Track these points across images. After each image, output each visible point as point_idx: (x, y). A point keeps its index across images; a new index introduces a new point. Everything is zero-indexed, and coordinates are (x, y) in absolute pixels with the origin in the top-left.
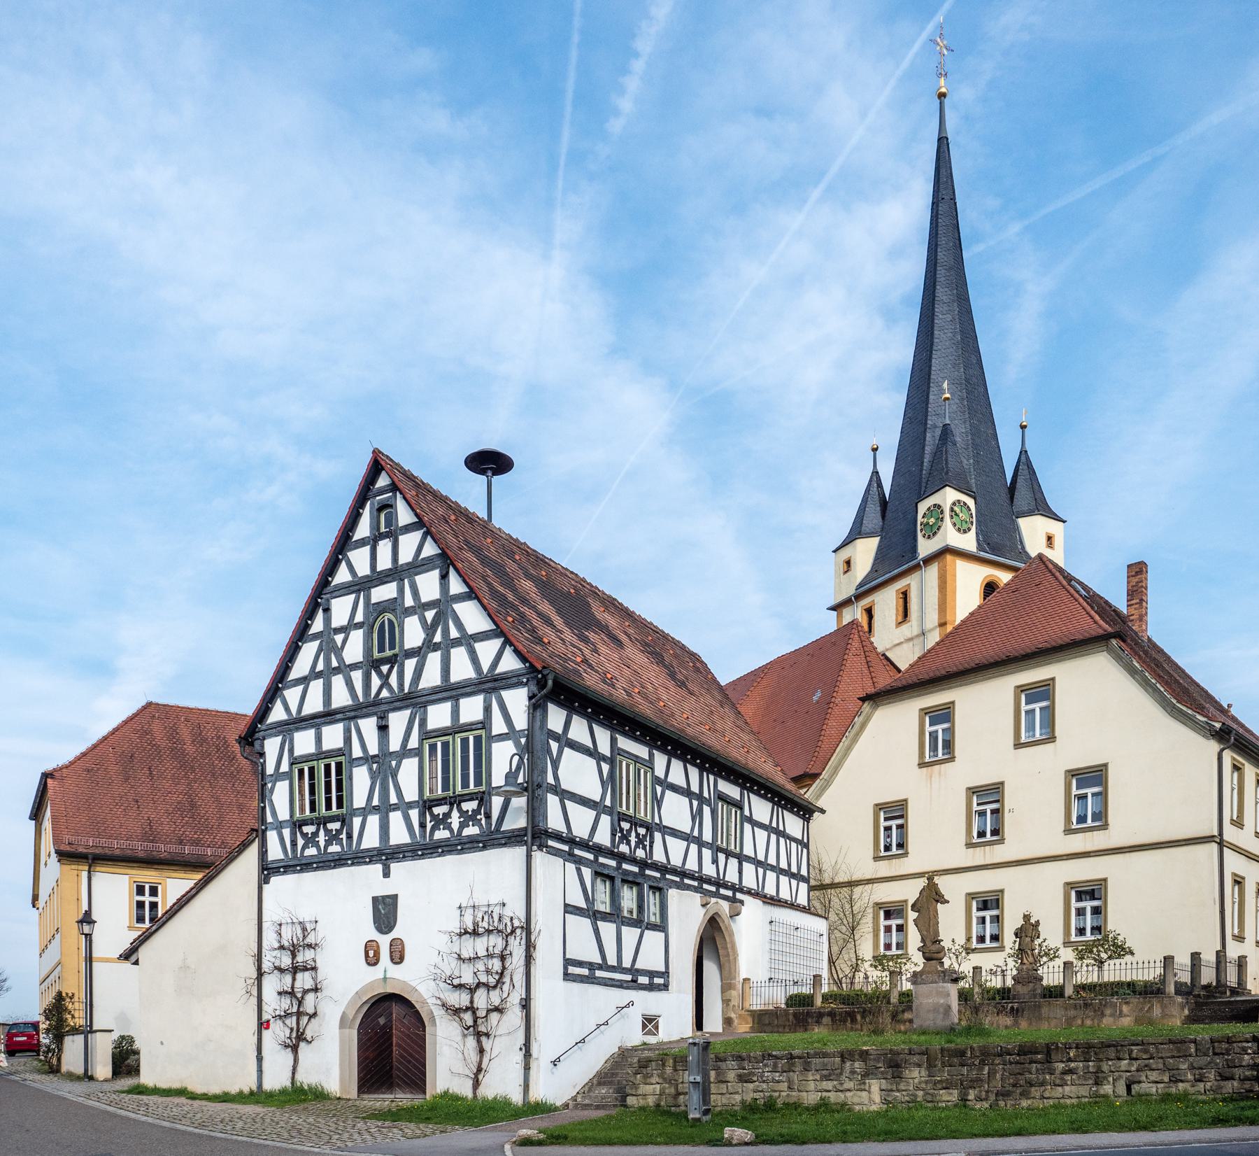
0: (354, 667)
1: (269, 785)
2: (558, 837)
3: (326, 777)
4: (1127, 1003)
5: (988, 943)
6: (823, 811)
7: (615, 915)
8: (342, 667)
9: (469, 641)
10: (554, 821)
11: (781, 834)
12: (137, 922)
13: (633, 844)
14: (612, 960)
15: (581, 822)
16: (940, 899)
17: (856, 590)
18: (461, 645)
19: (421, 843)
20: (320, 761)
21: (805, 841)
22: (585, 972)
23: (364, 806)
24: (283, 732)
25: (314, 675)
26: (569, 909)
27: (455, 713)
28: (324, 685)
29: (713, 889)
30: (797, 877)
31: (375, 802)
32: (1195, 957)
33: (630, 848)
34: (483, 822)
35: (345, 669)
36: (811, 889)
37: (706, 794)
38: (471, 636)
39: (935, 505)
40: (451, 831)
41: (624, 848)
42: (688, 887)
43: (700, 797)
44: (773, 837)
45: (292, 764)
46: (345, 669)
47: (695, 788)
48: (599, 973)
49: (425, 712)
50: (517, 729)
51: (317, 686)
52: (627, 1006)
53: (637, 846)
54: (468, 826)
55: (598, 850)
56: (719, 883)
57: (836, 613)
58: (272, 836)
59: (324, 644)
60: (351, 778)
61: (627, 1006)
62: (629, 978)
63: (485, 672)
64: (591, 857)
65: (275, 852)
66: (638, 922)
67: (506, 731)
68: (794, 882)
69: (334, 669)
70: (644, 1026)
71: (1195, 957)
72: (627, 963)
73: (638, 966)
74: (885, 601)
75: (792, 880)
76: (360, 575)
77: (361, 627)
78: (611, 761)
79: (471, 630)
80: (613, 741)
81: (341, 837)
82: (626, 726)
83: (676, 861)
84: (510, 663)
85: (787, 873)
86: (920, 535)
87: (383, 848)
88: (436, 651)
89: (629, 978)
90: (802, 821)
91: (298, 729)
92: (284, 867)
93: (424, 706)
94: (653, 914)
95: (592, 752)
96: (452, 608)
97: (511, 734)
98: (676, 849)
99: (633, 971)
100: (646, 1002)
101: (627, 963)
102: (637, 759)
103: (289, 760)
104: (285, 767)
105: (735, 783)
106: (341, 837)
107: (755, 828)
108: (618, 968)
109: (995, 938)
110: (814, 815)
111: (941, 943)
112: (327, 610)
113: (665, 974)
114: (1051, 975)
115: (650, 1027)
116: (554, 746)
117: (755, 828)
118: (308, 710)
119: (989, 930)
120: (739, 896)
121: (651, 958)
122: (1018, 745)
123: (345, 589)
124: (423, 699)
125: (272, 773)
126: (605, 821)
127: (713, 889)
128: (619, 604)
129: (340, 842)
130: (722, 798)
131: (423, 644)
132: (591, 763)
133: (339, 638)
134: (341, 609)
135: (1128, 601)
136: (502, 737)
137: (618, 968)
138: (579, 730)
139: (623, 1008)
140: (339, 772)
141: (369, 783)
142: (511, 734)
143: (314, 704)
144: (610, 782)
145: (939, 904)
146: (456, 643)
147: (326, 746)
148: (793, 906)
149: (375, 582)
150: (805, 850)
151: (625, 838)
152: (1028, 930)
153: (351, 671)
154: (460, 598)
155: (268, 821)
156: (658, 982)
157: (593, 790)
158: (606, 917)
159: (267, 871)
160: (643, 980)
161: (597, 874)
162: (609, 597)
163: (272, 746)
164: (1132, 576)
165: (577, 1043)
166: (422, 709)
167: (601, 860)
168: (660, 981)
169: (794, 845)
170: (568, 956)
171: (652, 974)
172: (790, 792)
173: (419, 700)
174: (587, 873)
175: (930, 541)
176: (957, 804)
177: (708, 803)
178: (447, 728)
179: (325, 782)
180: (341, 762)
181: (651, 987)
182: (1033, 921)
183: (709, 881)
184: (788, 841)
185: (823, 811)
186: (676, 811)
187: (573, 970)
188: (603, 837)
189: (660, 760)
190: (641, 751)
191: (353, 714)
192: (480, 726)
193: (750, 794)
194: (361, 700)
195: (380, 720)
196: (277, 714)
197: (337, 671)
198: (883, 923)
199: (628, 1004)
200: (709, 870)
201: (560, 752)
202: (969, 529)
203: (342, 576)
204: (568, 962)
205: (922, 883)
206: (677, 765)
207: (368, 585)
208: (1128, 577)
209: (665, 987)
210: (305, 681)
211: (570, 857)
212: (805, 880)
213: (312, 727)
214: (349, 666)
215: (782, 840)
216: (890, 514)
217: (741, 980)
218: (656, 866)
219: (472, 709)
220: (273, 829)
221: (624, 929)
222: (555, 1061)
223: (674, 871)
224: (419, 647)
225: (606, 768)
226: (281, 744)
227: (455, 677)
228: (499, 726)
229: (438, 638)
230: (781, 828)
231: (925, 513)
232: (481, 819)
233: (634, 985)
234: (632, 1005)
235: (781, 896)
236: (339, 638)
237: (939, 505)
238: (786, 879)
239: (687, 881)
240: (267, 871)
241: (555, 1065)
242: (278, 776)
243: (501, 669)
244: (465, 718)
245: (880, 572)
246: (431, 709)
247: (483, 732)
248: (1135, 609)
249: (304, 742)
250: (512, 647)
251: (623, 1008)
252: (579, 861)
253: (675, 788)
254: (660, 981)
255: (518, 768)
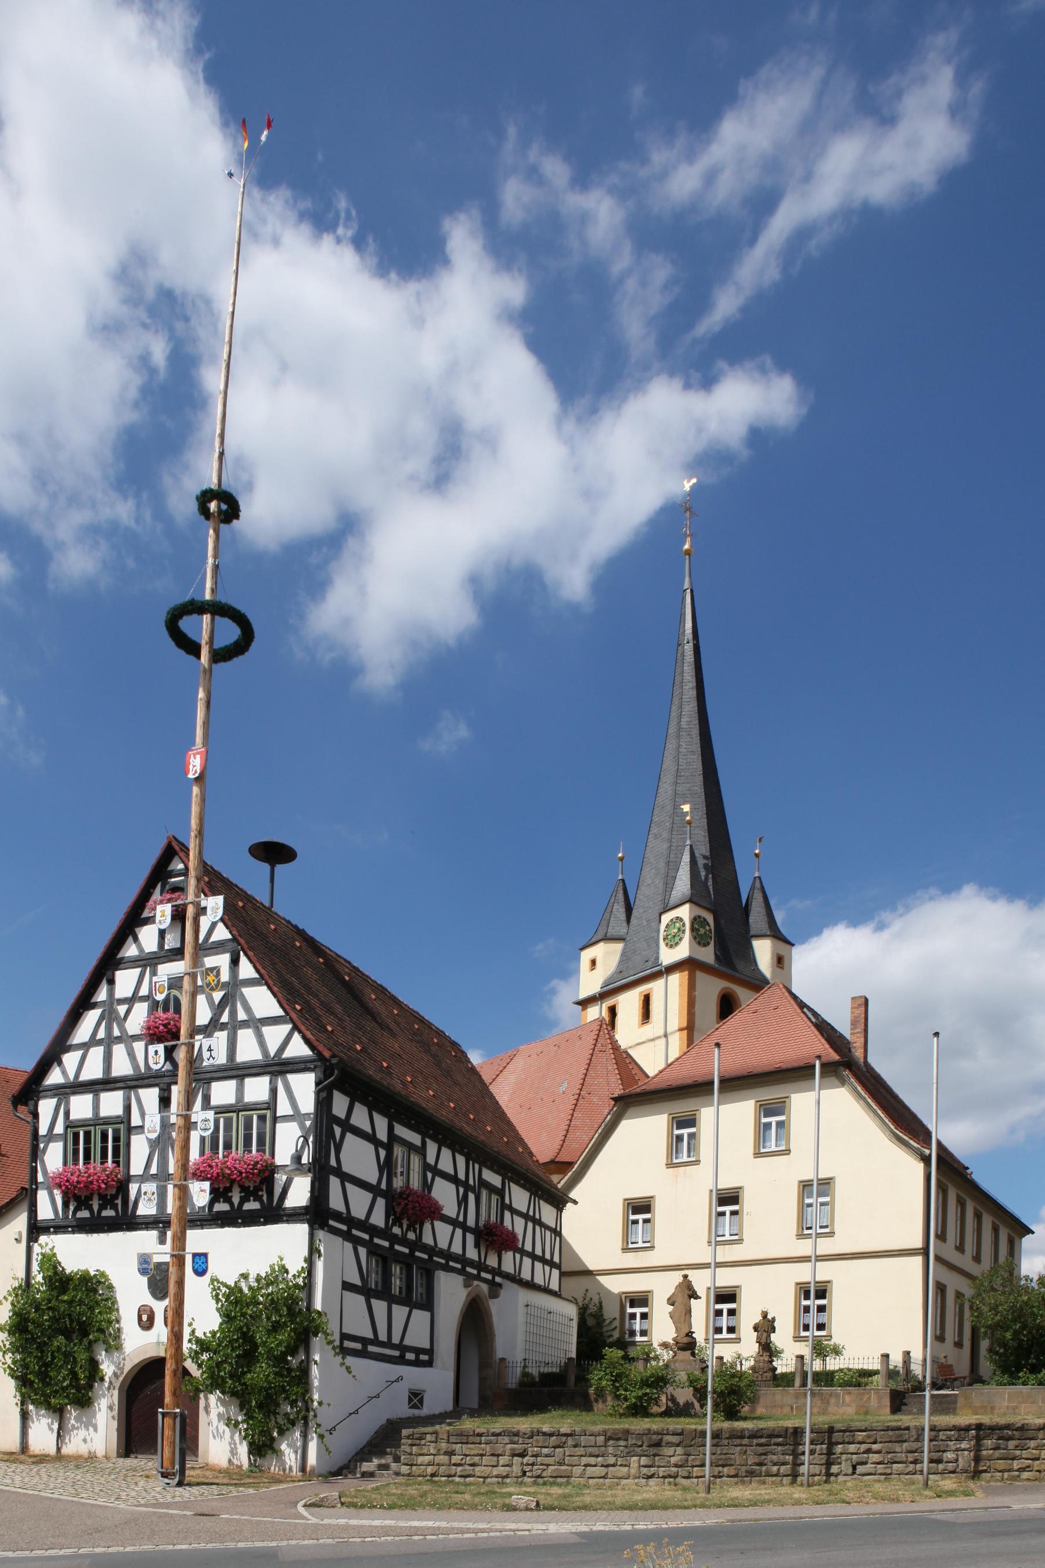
0: (135, 1038)
1: (42, 1146)
2: (337, 1216)
3: (102, 1142)
4: (849, 1393)
5: (725, 1335)
6: (575, 1202)
7: (384, 1293)
8: (124, 1037)
9: (257, 1024)
10: (336, 1202)
11: (538, 1222)
12: (793, 1386)
13: (405, 1227)
14: (383, 1337)
15: (359, 1203)
16: (694, 1295)
17: (602, 988)
18: (249, 1027)
19: (199, 1214)
20: (97, 1127)
21: (558, 1229)
22: (358, 1346)
23: (141, 1174)
24: (59, 1095)
25: (93, 1042)
26: (347, 1286)
27: (240, 1091)
28: (104, 1052)
29: (475, 1272)
30: (551, 1264)
31: (154, 1170)
32: (907, 1354)
33: (416, 1235)
34: (265, 1198)
35: (128, 1039)
36: (562, 1274)
37: (471, 1182)
38: (259, 1019)
39: (677, 918)
40: (232, 1204)
41: (396, 1230)
42: (453, 1270)
43: (465, 1184)
44: (530, 1225)
45: (66, 1128)
46: (128, 1039)
47: (462, 1176)
48: (371, 1348)
49: (209, 1089)
50: (303, 1112)
51: (97, 1054)
52: (397, 1380)
53: (408, 1229)
54: (249, 1201)
55: (373, 1231)
56: (481, 1266)
57: (581, 1007)
58: (42, 1196)
59: (107, 1013)
60: (128, 1145)
61: (397, 1380)
62: (397, 1353)
63: (272, 1055)
64: (366, 1237)
65: (45, 1211)
66: (406, 1300)
67: (292, 1113)
68: (547, 1268)
69: (117, 1038)
70: (410, 1400)
71: (907, 1354)
72: (396, 1340)
73: (407, 1342)
74: (628, 1003)
75: (545, 1266)
76: (147, 951)
77: (145, 1001)
78: (389, 1147)
79: (259, 1014)
80: (391, 1129)
81: (116, 1202)
82: (413, 1120)
83: (443, 1244)
84: (298, 1048)
85: (542, 1260)
86: (662, 944)
87: (160, 1216)
88: (223, 1030)
89: (397, 1353)
90: (556, 1210)
91: (74, 1093)
92: (54, 1227)
93: (208, 1081)
94: (418, 1291)
95: (371, 1138)
96: (242, 992)
97: (296, 1116)
98: (443, 1230)
99: (402, 1348)
100: (413, 1376)
101: (396, 1339)
102: (409, 1146)
103: (65, 1123)
104: (59, 1129)
105: (497, 1172)
106: (116, 1202)
107: (514, 1216)
108: (389, 1344)
109: (731, 1330)
110: (567, 1205)
111: (694, 1335)
112: (111, 982)
113: (430, 1352)
114: (784, 1365)
115: (415, 1401)
116: (338, 1131)
117: (514, 1216)
118: (86, 1076)
119: (724, 1322)
120: (498, 1279)
121: (417, 1337)
122: (758, 1154)
123: (134, 963)
124: (208, 1075)
125: (45, 1134)
126: (381, 1203)
127: (475, 1272)
128: (373, 981)
129: (114, 1207)
130: (484, 1184)
131: (210, 1023)
132: (371, 1147)
133: (122, 1009)
134: (125, 981)
135: (852, 1029)
136: (286, 1118)
137: (389, 1344)
138: (360, 1117)
139: (393, 1382)
140: (116, 1139)
141: (147, 1151)
142: (296, 1116)
143: (93, 1070)
144: (387, 1167)
145: (692, 1299)
146: (245, 1024)
147: (104, 1113)
148: (546, 1290)
149: (162, 960)
150: (558, 1239)
151: (398, 1222)
152: (766, 1327)
153: (133, 1042)
154: (250, 983)
155: (39, 1181)
156: (424, 1358)
157: (371, 1175)
158: (379, 1296)
159: (36, 1229)
160: (410, 1356)
161: (370, 1253)
162: (381, 986)
163: (46, 1107)
164: (855, 1008)
165: (351, 1414)
166: (206, 1085)
167: (376, 1241)
168: (424, 1357)
169: (548, 1233)
170: (344, 1331)
171: (418, 1351)
172: (537, 1176)
173: (203, 1076)
174: (363, 1251)
175: (672, 951)
176: (702, 1205)
177: (472, 1189)
178: (231, 1105)
179: (101, 1147)
180: (119, 1130)
181: (417, 1363)
182: (769, 1317)
183: (471, 1263)
184: (543, 1229)
185: (575, 1202)
186: (445, 1194)
187: (348, 1344)
188: (378, 1219)
189: (432, 1148)
190: (415, 1138)
191: (134, 1083)
192: (265, 1106)
193: (511, 1183)
194: (143, 1071)
195: (162, 1092)
196: (55, 1077)
197: (119, 1040)
198: (725, 1335)
199: (398, 1379)
200: (472, 1254)
201: (343, 1136)
202: (708, 944)
203: (130, 951)
204: (344, 1337)
205: (677, 1277)
206: (446, 1154)
207: (156, 961)
208: (852, 1008)
209: (429, 1364)
210: (86, 1047)
211: (347, 1236)
212: (558, 1266)
213: (91, 1092)
214: (132, 1036)
215: (538, 1228)
216: (635, 921)
217: (498, 1361)
218: (425, 1248)
219: (257, 1089)
220: (43, 1189)
221: (395, 1307)
222: (331, 1430)
223: (442, 1253)
224: (205, 1026)
225: (383, 1153)
226: (56, 1106)
227: (242, 1057)
228: (283, 1108)
229: (225, 1018)
230: (537, 1216)
231: (668, 924)
232: (263, 1195)
233: (401, 1360)
234: (402, 1380)
235: (522, 1276)
236: (122, 1009)
237: (681, 918)
238: (541, 1265)
239: (451, 1264)
240: (36, 1229)
241: (331, 1434)
242: (51, 1137)
243: (288, 1054)
244: (249, 1097)
245: (625, 974)
246: (215, 1085)
247: (268, 1113)
248: (858, 1037)
249: (81, 1107)
250: (535, 1159)
251: (393, 1382)
252: (356, 1242)
253: (445, 1176)
254: (424, 1357)
255: (303, 1147)
